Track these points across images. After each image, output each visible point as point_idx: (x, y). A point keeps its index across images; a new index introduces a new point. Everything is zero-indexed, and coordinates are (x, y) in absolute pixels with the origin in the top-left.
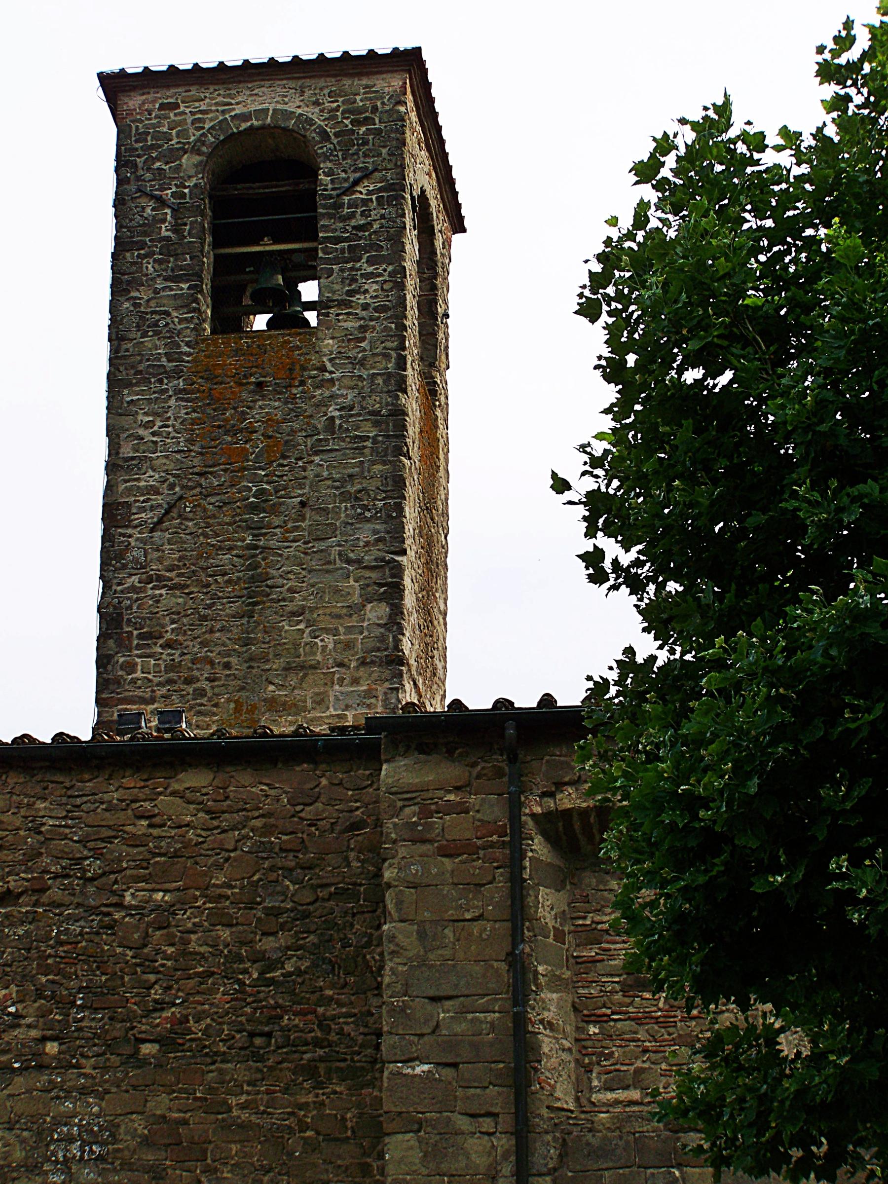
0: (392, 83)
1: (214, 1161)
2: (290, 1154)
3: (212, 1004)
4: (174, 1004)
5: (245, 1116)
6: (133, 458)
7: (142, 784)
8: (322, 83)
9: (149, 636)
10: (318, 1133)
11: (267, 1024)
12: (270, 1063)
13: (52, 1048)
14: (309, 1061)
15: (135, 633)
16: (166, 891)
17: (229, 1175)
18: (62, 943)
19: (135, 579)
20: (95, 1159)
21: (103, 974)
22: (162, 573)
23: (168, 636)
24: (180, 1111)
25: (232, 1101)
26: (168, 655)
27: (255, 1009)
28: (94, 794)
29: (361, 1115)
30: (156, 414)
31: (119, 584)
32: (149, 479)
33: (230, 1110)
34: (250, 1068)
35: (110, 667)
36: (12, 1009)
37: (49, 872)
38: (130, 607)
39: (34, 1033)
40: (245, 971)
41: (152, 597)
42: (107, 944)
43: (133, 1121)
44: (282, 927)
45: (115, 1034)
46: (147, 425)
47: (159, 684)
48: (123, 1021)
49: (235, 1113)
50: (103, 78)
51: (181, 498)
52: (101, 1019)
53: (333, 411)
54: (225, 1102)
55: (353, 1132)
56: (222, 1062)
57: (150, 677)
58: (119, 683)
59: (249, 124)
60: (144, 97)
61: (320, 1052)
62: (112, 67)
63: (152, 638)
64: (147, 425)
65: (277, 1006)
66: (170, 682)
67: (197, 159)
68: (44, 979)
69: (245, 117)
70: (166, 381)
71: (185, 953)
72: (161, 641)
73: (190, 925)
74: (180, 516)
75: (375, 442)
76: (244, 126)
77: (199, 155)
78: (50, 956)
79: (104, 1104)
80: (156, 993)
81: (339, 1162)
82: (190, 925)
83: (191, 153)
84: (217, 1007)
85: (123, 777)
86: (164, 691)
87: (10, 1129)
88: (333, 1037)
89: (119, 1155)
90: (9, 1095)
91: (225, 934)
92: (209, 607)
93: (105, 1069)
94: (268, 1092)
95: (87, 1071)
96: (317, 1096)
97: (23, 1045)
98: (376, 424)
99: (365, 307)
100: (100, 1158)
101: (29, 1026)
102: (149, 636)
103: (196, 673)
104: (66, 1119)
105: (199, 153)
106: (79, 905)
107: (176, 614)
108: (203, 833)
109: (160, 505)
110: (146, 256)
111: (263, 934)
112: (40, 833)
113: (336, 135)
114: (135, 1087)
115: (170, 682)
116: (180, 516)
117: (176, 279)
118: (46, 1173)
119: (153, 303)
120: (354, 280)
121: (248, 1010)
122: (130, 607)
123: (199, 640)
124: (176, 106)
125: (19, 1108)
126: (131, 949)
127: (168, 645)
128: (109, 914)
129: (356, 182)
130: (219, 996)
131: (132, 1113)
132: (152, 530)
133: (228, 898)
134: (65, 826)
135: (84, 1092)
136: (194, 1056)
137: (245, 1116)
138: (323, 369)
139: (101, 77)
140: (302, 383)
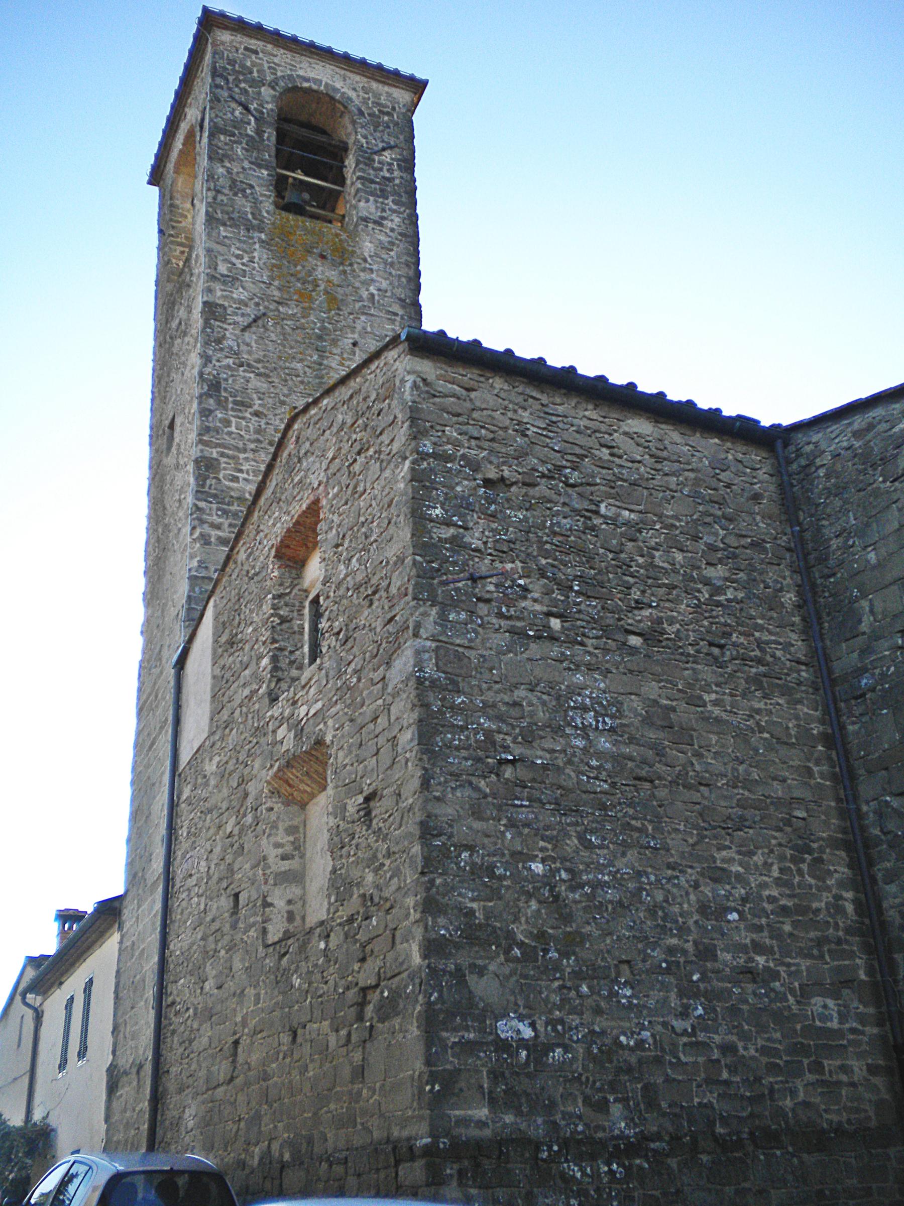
0: (402, 96)
1: (700, 747)
2: (756, 750)
3: (679, 612)
4: (651, 606)
5: (717, 711)
6: (228, 276)
7: (601, 419)
9: (242, 404)
10: (772, 736)
11: (723, 638)
12: (729, 670)
13: (555, 623)
14: (756, 674)
15: (231, 399)
16: (631, 511)
17: (713, 762)
18: (555, 534)
19: (231, 361)
20: (609, 730)
21: (591, 568)
23: (256, 407)
24: (668, 698)
25: (706, 697)
27: (712, 623)
28: (566, 417)
29: (798, 726)
30: (244, 251)
31: (218, 361)
32: (239, 294)
33: (705, 706)
34: (714, 672)
35: (211, 419)
36: (521, 582)
37: (537, 471)
38: (226, 380)
39: (538, 607)
40: (699, 591)
41: (244, 377)
42: (590, 542)
43: (632, 700)
44: (720, 561)
45: (608, 621)
46: (238, 257)
47: (249, 440)
48: (613, 612)
49: (709, 708)
51: (264, 314)
52: (595, 607)
53: (372, 289)
54: (700, 698)
55: (797, 739)
56: (694, 662)
57: (242, 433)
58: (218, 433)
61: (762, 669)
64: (238, 257)
65: (726, 625)
67: (272, 92)
68: (544, 562)
69: (307, 80)
71: (652, 565)
72: (250, 410)
73: (653, 544)
75: (402, 318)
76: (306, 85)
78: (547, 542)
79: (607, 681)
80: (636, 594)
81: (791, 763)
82: (653, 544)
84: (683, 615)
85: (586, 410)
86: (253, 446)
87: (532, 690)
88: (769, 658)
89: (626, 729)
90: (528, 659)
91: (679, 557)
93: (606, 651)
94: (732, 695)
95: (591, 649)
96: (766, 704)
97: (535, 616)
98: (403, 307)
99: (392, 230)
100: (612, 730)
101: (535, 600)
102: (242, 404)
104: (578, 690)
105: (273, 88)
106: (564, 504)
107: (262, 395)
108: (653, 472)
109: (249, 315)
110: (235, 142)
111: (707, 564)
112: (526, 436)
113: (369, 115)
114: (631, 672)
115: (258, 441)
116: (264, 326)
117: (260, 166)
118: (568, 736)
119: (241, 176)
120: (383, 210)
121: (706, 623)
122: (226, 380)
124: (256, 52)
125: (538, 672)
126: (611, 551)
127: (257, 414)
128: (590, 519)
129: (384, 149)
130: (683, 607)
131: (631, 694)
133: (677, 528)
134: (545, 436)
135: (590, 668)
136: (672, 654)
137: (717, 711)
138: (365, 260)
139: (205, 10)
140: (351, 265)
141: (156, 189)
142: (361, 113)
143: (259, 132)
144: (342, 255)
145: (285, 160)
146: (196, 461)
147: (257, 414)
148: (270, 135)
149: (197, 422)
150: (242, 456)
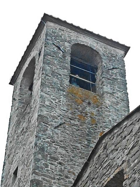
8: (103, 44)
22: (58, 141)
23: (60, 161)
26: (60, 166)
46: (53, 99)
50: (9, 84)
53: (110, 118)
59: (84, 43)
60: (55, 25)
62: (46, 13)
63: (54, 159)
64: (53, 99)
66: (60, 175)
69: (83, 42)
70: (60, 91)
72: (57, 161)
74: (64, 127)
77: (70, 43)
83: (68, 42)
86: (58, 177)
92: (73, 157)
103: (69, 176)
107: (63, 155)
123: (70, 166)
127: (60, 163)
129: (113, 68)
132: (55, 128)
141: (13, 87)
142: (104, 55)
143: (64, 56)
144: (98, 105)
145: (73, 71)
146: (32, 181)
147: (60, 163)
148: (68, 58)
149: (32, 164)
150: (53, 181)
